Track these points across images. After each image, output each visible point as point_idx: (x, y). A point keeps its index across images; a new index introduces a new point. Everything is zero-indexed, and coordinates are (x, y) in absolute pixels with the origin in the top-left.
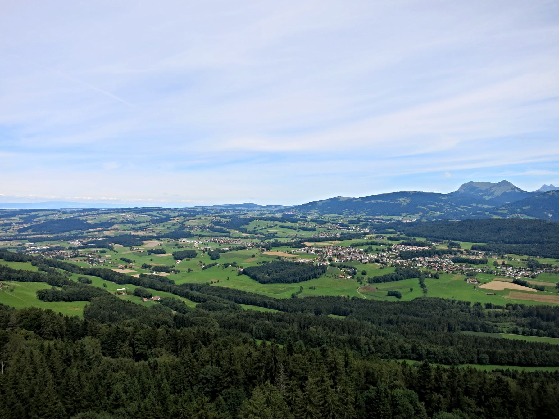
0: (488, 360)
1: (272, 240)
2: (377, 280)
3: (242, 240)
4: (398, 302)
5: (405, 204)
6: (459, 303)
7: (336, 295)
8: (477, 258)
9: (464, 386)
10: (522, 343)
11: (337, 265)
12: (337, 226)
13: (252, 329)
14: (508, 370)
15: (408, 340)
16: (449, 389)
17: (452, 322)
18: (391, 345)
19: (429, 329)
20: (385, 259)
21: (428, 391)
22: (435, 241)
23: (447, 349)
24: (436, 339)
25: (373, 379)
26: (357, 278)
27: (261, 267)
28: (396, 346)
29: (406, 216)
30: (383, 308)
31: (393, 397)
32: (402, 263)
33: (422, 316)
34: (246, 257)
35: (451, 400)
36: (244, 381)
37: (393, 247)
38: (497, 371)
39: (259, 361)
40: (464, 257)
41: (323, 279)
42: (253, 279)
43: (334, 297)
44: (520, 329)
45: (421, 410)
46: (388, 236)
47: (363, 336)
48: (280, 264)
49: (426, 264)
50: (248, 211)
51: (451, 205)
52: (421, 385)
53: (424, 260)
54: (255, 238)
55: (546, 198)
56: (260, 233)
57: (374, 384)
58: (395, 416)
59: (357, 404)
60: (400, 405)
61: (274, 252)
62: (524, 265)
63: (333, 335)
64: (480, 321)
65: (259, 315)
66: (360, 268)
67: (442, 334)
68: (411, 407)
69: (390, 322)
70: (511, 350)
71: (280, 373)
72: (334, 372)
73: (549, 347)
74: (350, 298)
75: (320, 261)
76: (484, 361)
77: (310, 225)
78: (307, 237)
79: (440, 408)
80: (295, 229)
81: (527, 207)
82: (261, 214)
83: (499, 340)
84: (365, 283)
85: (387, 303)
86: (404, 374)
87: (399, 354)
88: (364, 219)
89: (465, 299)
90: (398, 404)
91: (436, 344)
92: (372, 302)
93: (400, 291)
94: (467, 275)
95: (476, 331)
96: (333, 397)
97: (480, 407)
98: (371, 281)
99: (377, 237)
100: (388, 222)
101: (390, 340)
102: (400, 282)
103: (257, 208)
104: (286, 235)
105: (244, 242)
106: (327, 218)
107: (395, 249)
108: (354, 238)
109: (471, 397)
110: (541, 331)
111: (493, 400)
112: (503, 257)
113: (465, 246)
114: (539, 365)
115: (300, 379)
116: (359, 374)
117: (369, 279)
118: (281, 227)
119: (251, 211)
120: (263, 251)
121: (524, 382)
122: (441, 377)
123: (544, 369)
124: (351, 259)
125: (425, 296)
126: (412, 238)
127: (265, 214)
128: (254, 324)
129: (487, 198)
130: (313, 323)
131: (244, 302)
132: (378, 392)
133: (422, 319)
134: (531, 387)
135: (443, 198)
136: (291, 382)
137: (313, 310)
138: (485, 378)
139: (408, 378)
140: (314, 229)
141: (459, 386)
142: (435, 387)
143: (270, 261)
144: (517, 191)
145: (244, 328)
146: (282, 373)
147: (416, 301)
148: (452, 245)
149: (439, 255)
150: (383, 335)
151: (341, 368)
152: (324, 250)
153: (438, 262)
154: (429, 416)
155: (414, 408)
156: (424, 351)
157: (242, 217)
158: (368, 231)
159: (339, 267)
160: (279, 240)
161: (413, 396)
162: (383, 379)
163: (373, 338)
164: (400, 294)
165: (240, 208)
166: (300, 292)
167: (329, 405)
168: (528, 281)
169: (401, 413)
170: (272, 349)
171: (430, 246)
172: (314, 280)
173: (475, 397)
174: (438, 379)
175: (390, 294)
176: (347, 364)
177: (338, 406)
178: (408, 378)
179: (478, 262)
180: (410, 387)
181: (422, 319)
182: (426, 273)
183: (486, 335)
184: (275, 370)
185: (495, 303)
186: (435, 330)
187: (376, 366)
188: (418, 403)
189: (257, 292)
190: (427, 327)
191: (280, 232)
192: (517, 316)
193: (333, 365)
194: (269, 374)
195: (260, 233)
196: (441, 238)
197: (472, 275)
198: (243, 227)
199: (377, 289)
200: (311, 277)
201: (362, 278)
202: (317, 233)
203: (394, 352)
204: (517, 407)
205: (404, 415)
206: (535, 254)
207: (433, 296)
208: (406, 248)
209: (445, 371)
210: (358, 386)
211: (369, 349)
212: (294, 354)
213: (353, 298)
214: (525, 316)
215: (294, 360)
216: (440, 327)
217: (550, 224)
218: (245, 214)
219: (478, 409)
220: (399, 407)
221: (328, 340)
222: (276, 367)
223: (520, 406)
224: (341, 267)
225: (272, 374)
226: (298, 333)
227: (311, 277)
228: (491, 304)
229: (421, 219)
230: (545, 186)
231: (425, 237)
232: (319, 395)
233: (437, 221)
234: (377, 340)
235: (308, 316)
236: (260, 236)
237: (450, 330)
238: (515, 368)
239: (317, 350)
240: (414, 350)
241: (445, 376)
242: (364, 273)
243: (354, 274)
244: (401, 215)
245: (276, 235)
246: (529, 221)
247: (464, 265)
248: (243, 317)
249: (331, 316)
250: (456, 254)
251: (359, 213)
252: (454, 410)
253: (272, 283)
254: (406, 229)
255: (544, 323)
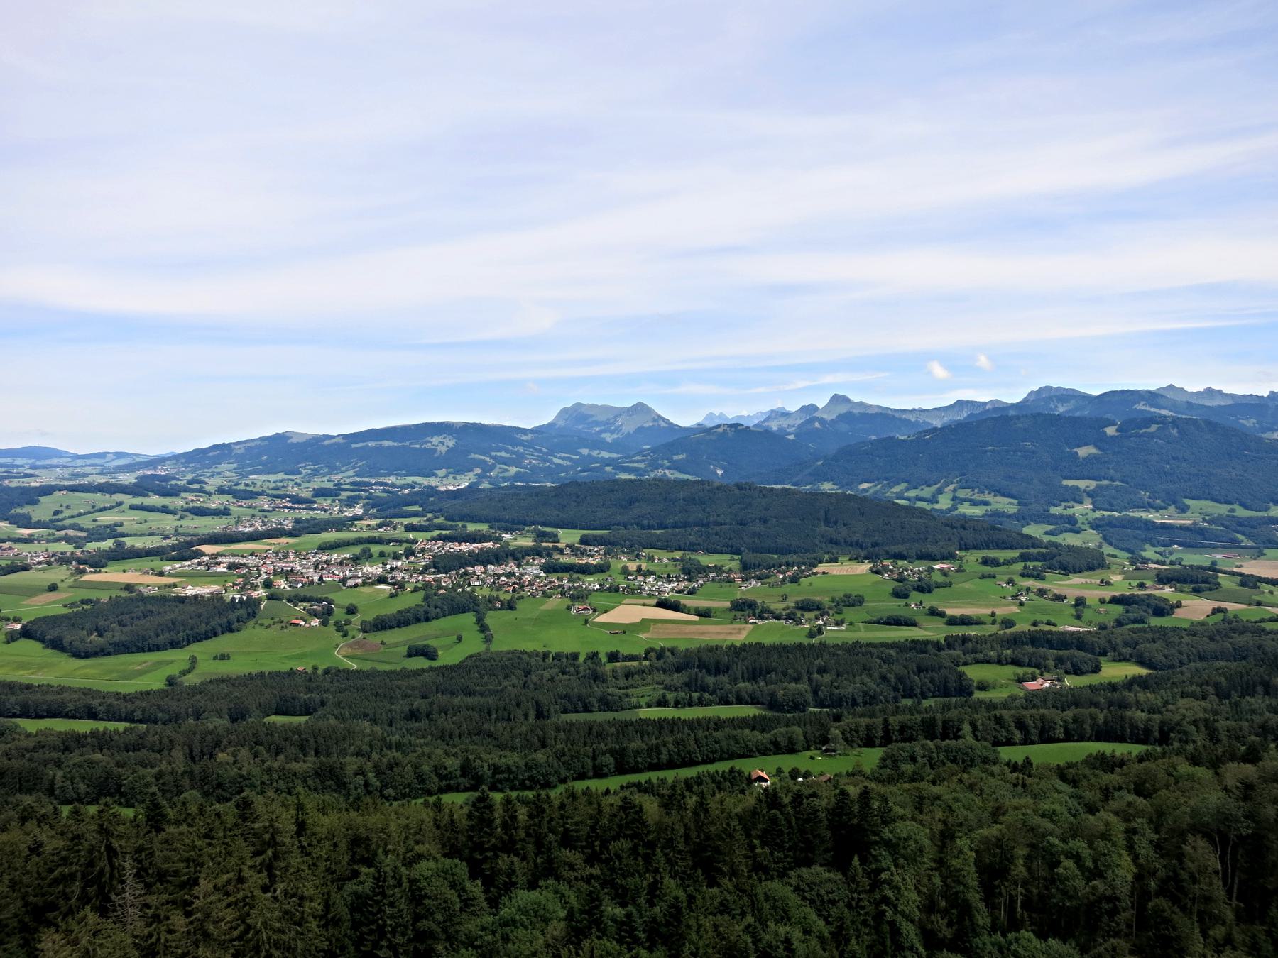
0: (612, 767)
1: (108, 544)
2: (381, 625)
3: (18, 547)
4: (431, 669)
5: (443, 449)
6: (558, 657)
7: (285, 667)
8: (590, 560)
9: (561, 829)
10: (674, 723)
11: (287, 595)
12: (286, 502)
13: (53, 782)
14: (649, 781)
15: (454, 750)
16: (532, 840)
17: (543, 698)
18: (416, 767)
19: (497, 719)
20: (399, 575)
21: (489, 854)
22: (507, 530)
23: (534, 756)
24: (512, 738)
25: (368, 851)
26: (336, 623)
27: (76, 614)
28: (426, 768)
29: (446, 476)
30: (399, 687)
31: (412, 881)
32: (438, 581)
33: (482, 694)
34: (32, 591)
35: (535, 862)
36: (20, 921)
37: (419, 546)
38: (629, 786)
39: (65, 861)
40: (565, 560)
41: (251, 633)
42: (54, 647)
43: (278, 673)
44: (670, 696)
45: (474, 899)
46: (406, 521)
47: (352, 755)
48: (132, 603)
49: (489, 580)
50: (34, 467)
51: (540, 451)
52: (474, 843)
53: (485, 572)
54: (59, 540)
55: (713, 438)
56: (72, 527)
57: (369, 862)
58: (419, 924)
59: (330, 916)
60: (429, 898)
61: (113, 575)
62: (675, 571)
63: (276, 765)
64: (598, 690)
65: (72, 742)
66: (342, 599)
67: (525, 725)
68: (452, 895)
69: (413, 715)
70: (654, 741)
71: (123, 882)
72: (270, 852)
73: (719, 724)
74: (320, 672)
75: (242, 589)
76: (606, 770)
77: (215, 503)
78: (206, 531)
79: (514, 884)
80: (173, 513)
81: (681, 457)
82: (76, 476)
83: (631, 723)
84: (354, 633)
85: (406, 674)
86: (438, 827)
87: (434, 782)
88: (351, 484)
89: (568, 649)
90: (426, 896)
91: (513, 749)
92: (372, 674)
93: (433, 643)
94: (572, 597)
95: (591, 711)
96: (266, 912)
97: (592, 866)
98: (368, 628)
99: (380, 526)
100: (407, 491)
101: (412, 757)
102: (435, 624)
103: (62, 461)
104: (141, 526)
105: (25, 551)
106: (259, 483)
107: (423, 550)
108: (326, 530)
109: (575, 848)
110: (706, 695)
111: (615, 846)
112: (638, 556)
113: (568, 537)
114: (705, 762)
115: (183, 886)
116: (335, 845)
117: (363, 622)
118: (133, 507)
119: (44, 467)
120: (84, 572)
121: (670, 801)
122: (514, 818)
123: (711, 768)
124: (321, 579)
125: (488, 649)
126: (460, 524)
127: (86, 475)
128: (59, 767)
129: (609, 437)
130: (225, 742)
131: (26, 714)
132: (379, 879)
133: (482, 700)
134: (682, 807)
135: (524, 438)
136: (152, 899)
137: (225, 711)
138: (599, 805)
139: (448, 834)
140: (225, 512)
141: (551, 830)
142: (503, 842)
143: (104, 597)
144: (663, 424)
145: (27, 783)
146: (130, 880)
147: (469, 662)
148: (541, 536)
149: (515, 559)
150: (399, 746)
151: (287, 841)
152: (251, 561)
153: (513, 574)
154: (491, 907)
155: (459, 896)
156: (486, 768)
157: (14, 483)
158: (360, 512)
159: (289, 601)
160: (129, 542)
161: (458, 870)
162: (389, 847)
163: (375, 756)
164: (435, 651)
165: (9, 460)
166: (189, 671)
167: (257, 933)
168: (683, 602)
169: (432, 913)
170: (101, 826)
171: (497, 540)
172: (228, 636)
173: (582, 847)
174: (510, 823)
175: (414, 652)
176: (301, 827)
177: (281, 931)
178: (448, 834)
179: (592, 570)
180: (452, 851)
181: (482, 700)
182: (490, 600)
183: (610, 716)
184: (112, 877)
185: (625, 650)
186: (509, 719)
187: (375, 820)
188: (468, 884)
189: (66, 682)
190: (494, 716)
191: (129, 520)
192: (664, 672)
193: (267, 836)
194: (92, 890)
195: (72, 527)
196: (519, 523)
197: (580, 596)
198: (19, 510)
199: (383, 643)
200: (219, 630)
201: (348, 622)
202: (233, 521)
203: (423, 781)
204: (658, 850)
205: (439, 917)
206: (693, 548)
207: (505, 648)
208: (447, 548)
209: (524, 802)
210: (333, 872)
211: (366, 785)
212: (166, 826)
213: (327, 672)
214: (678, 670)
215: (167, 841)
216: (519, 712)
217: (719, 488)
218: (26, 476)
219: (589, 870)
220: (427, 901)
221: (266, 778)
222: (112, 867)
223: (663, 849)
224: (295, 599)
225: (101, 888)
226: (185, 772)
227: (219, 630)
228: (617, 652)
229: (479, 483)
230: (710, 416)
231: (487, 521)
232: (230, 915)
233: (512, 486)
234: (385, 760)
235: (211, 727)
236: (71, 533)
237: (540, 715)
238: (661, 774)
239: (228, 810)
240: (466, 769)
241: (522, 814)
242: (351, 610)
243: (326, 612)
244: (436, 475)
245: (119, 529)
246: (685, 483)
247: (566, 576)
248: (22, 753)
249: (273, 718)
250: (549, 555)
251: (334, 470)
252: (541, 883)
253: (109, 654)
254: (447, 504)
255: (710, 680)
